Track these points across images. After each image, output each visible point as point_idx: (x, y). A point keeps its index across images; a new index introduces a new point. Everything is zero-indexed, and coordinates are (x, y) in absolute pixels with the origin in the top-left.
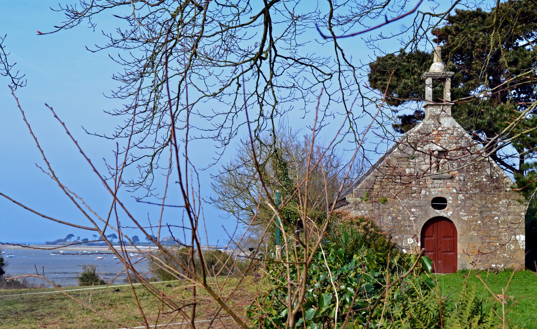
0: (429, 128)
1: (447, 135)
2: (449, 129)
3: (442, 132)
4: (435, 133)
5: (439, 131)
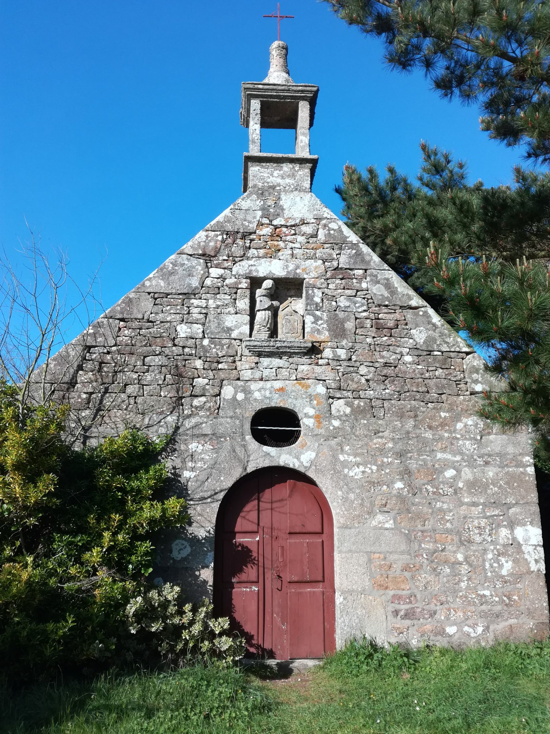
0: (249, 218)
1: (300, 239)
2: (304, 222)
3: (284, 229)
4: (267, 231)
5: (276, 227)
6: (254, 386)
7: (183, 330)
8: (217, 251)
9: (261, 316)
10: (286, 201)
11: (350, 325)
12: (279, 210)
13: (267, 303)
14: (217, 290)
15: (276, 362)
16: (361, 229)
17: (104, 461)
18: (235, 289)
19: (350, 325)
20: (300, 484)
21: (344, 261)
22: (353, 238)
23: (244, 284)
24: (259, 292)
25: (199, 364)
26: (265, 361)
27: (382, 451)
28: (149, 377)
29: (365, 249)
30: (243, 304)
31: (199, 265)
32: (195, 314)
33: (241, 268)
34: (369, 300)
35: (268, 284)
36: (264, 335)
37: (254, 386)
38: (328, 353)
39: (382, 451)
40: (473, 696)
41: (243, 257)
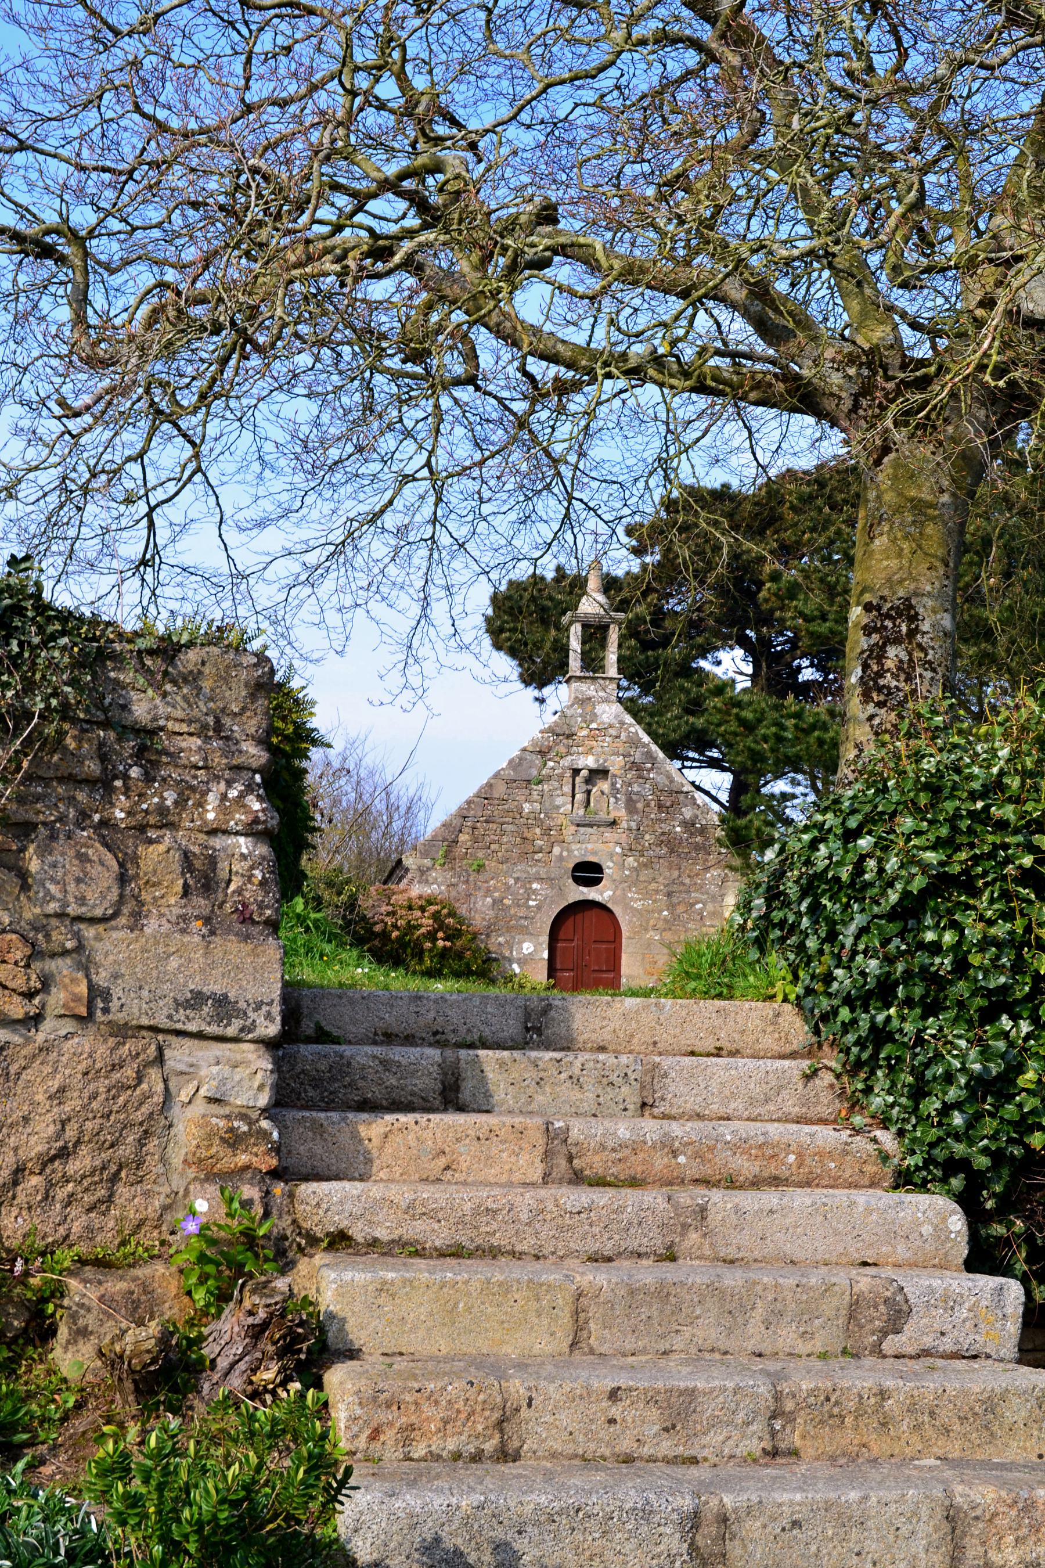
2: (611, 726)
6: (574, 847)
7: (527, 807)
8: (550, 749)
9: (579, 797)
10: (599, 709)
11: (640, 805)
12: (594, 717)
13: (584, 787)
14: (550, 777)
15: (589, 830)
16: (680, 950)
17: (948, 1192)
18: (561, 777)
19: (640, 805)
20: (604, 913)
21: (638, 757)
22: (646, 739)
23: (568, 774)
24: (578, 780)
25: (538, 831)
26: (582, 830)
27: (657, 892)
28: (505, 839)
29: (654, 747)
30: (568, 789)
31: (538, 761)
32: (535, 796)
33: (566, 762)
34: (655, 786)
35: (584, 773)
36: (581, 812)
37: (574, 847)
38: (624, 825)
39: (657, 892)
40: (920, 301)
41: (568, 753)
